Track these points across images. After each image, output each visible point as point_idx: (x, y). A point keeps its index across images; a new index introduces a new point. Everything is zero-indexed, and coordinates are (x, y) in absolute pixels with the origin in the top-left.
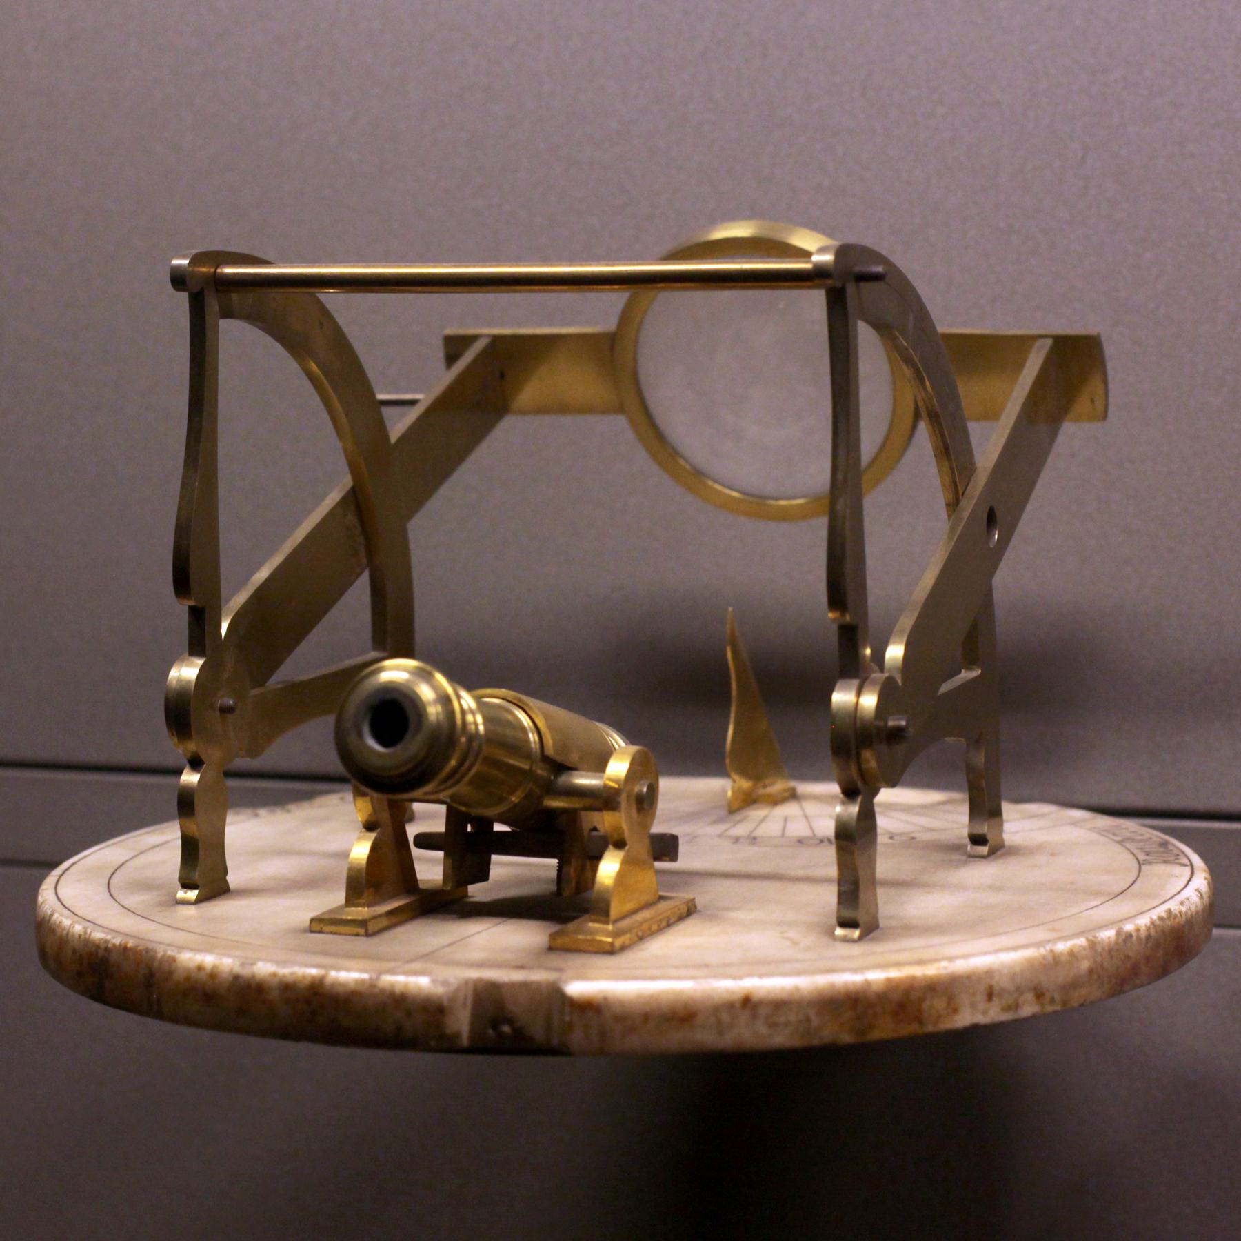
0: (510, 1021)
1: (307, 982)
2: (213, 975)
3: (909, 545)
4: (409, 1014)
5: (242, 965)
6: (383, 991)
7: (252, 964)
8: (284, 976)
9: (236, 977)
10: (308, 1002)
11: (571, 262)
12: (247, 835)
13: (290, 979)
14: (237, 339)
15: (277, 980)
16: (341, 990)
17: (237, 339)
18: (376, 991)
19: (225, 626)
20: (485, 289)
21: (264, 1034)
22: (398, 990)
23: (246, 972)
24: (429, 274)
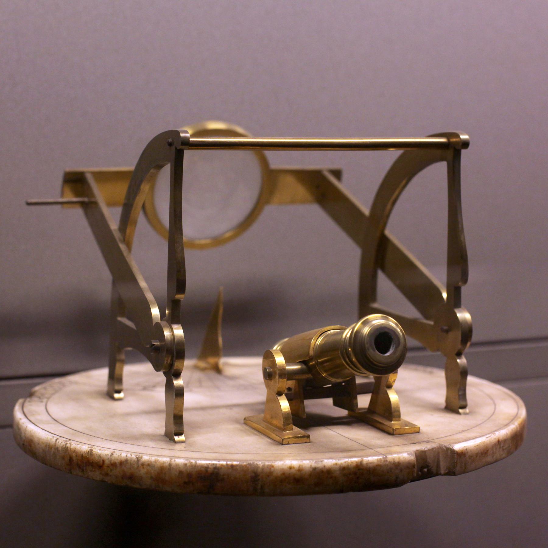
0: (427, 466)
1: (354, 464)
2: (300, 470)
3: (148, 262)
4: (401, 470)
5: (316, 462)
6: (390, 462)
7: (322, 461)
8: (342, 464)
9: (315, 469)
10: (355, 473)
11: (421, 137)
12: (477, 387)
13: (345, 465)
14: (438, 171)
15: (338, 467)
16: (371, 465)
17: (438, 171)
18: (387, 463)
19: (445, 295)
20: (308, 149)
21: (329, 493)
22: (396, 461)
23: (320, 465)
24: (364, 142)
